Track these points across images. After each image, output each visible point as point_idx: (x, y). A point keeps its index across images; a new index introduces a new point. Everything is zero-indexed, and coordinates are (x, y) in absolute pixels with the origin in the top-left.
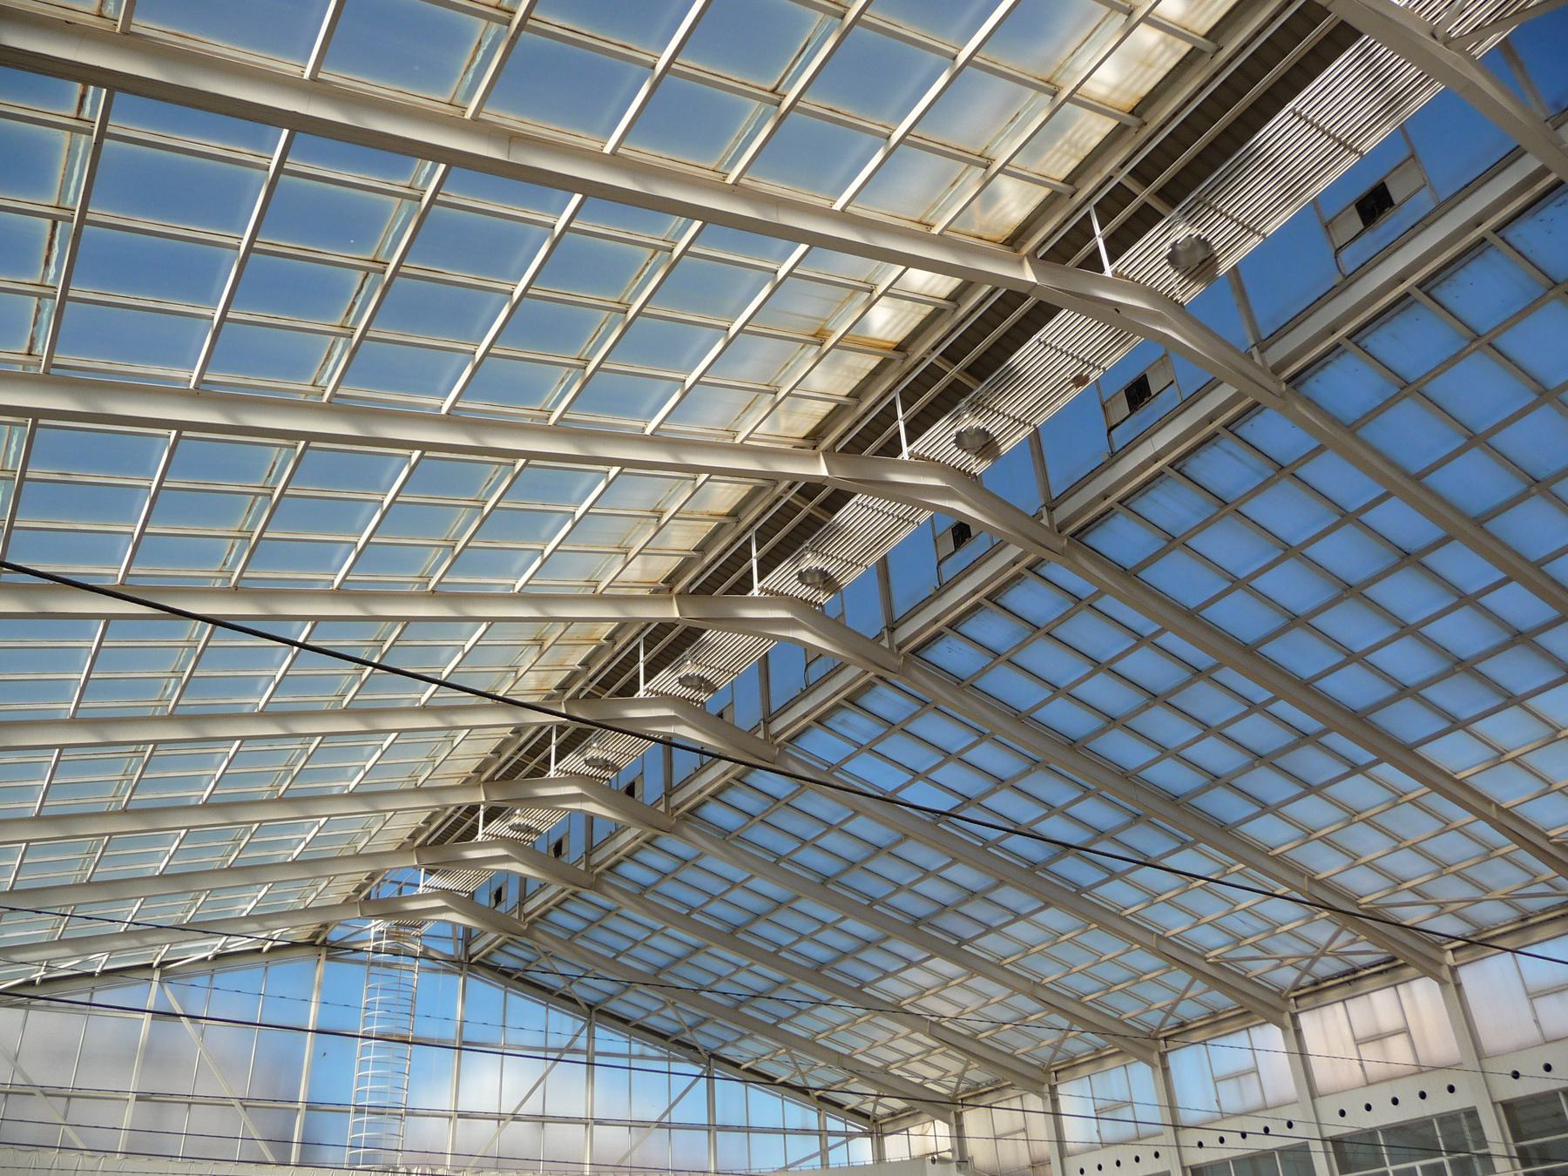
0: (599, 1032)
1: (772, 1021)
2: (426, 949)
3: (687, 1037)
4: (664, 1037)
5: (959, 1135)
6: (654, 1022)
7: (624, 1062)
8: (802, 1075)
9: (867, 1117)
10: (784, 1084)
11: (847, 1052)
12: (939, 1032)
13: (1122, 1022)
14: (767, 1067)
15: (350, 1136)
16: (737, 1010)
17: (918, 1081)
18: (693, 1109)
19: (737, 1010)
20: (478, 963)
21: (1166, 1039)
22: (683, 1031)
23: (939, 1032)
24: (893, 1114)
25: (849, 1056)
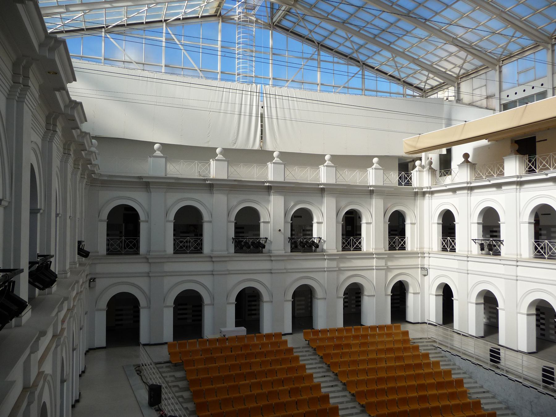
0: (322, 53)
1: (388, 44)
2: (257, 19)
3: (355, 55)
5: (458, 91)
6: (342, 49)
7: (332, 72)
9: (422, 90)
11: (416, 57)
13: (472, 47)
14: (384, 68)
15: (237, 72)
17: (444, 70)
20: (276, 25)
22: (353, 53)
24: (441, 84)
25: (417, 59)
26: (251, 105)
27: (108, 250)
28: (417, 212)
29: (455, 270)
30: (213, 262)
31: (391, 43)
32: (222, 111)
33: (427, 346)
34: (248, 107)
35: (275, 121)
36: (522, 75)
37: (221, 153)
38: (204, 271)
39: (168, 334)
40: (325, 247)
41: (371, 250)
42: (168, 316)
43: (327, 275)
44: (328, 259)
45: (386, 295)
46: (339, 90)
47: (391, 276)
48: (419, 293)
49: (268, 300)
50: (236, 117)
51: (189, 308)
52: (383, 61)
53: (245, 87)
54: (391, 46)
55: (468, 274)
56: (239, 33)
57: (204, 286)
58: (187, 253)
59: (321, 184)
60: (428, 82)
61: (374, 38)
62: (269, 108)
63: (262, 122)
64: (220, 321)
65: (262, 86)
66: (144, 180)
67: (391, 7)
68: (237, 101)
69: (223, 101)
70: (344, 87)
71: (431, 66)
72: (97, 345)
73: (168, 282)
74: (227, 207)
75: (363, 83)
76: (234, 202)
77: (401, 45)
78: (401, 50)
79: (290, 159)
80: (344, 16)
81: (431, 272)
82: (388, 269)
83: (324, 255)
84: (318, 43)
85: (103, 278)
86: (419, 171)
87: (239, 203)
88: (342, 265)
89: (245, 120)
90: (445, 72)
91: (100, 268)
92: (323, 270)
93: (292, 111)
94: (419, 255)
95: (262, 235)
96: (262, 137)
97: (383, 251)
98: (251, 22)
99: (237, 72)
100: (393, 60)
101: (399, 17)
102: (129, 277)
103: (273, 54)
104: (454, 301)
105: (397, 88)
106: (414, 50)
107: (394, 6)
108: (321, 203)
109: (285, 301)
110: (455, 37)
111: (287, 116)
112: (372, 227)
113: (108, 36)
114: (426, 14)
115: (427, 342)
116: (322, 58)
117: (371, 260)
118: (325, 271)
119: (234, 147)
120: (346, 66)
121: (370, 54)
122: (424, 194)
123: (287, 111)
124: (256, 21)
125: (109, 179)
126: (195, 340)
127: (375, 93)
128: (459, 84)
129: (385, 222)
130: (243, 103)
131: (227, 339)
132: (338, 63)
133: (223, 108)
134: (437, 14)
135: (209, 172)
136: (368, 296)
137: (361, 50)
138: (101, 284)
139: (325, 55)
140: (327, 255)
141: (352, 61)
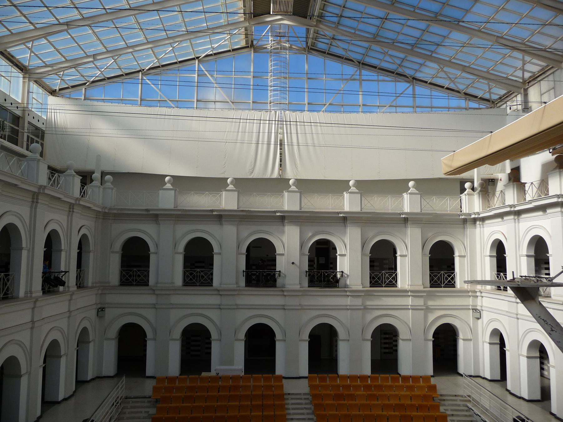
0: (364, 72)
2: (291, 45)
3: (400, 70)
4: (393, 73)
11: (467, 65)
13: (524, 44)
15: (269, 100)
16: (413, 48)
19: (413, 48)
24: (500, 98)
25: (469, 67)
26: (270, 133)
27: (184, 281)
28: (467, 243)
29: (505, 313)
30: (221, 295)
31: (432, 52)
33: (459, 405)
34: (266, 134)
35: (296, 147)
37: (354, 186)
38: (268, 305)
39: (304, 370)
40: (348, 283)
41: (407, 287)
42: (240, 350)
43: (352, 312)
44: (412, 296)
45: (364, 340)
46: (384, 109)
47: (432, 317)
48: (471, 340)
49: (281, 338)
50: (254, 146)
51: (196, 342)
52: (433, 73)
53: (257, 115)
54: (434, 55)
55: (518, 319)
56: (271, 61)
57: (212, 320)
58: (197, 286)
59: (403, 214)
60: (492, 91)
61: (412, 49)
62: (289, 134)
63: (281, 149)
64: (354, 358)
66: (151, 212)
67: (415, 12)
68: (255, 130)
69: (240, 131)
70: (390, 106)
71: (488, 72)
72: (104, 374)
73: (174, 315)
74: (237, 239)
75: (414, 101)
76: (245, 233)
77: (444, 53)
78: (447, 59)
79: (306, 186)
80: (373, 30)
81: (485, 315)
82: (428, 310)
83: (346, 291)
84: (359, 63)
85: (112, 307)
86: (468, 194)
87: (251, 234)
88: (368, 303)
89: (262, 149)
91: (111, 298)
92: (345, 307)
93: (314, 135)
94: (470, 294)
96: (281, 165)
97: (421, 288)
98: (285, 48)
99: (269, 100)
100: (442, 70)
101: (428, 23)
102: (139, 308)
103: (308, 78)
104: (507, 352)
105: (457, 102)
106: (460, 56)
107: (417, 11)
108: (345, 233)
109: (300, 340)
111: (310, 142)
112: (407, 260)
113: (145, 78)
114: (457, 14)
115: (461, 401)
116: (364, 78)
118: (409, 309)
119: (251, 177)
120: (394, 83)
121: (416, 67)
122: (475, 220)
123: (309, 136)
124: (290, 48)
125: (119, 212)
126: (378, 375)
127: (430, 109)
128: (526, 90)
129: (363, 254)
130: (261, 131)
131: (220, 378)
132: (384, 81)
133: (239, 138)
134: (467, 11)
135: (220, 203)
136: (403, 340)
137: (404, 64)
138: (110, 313)
139: (367, 73)
140: (350, 291)
141: (403, 77)
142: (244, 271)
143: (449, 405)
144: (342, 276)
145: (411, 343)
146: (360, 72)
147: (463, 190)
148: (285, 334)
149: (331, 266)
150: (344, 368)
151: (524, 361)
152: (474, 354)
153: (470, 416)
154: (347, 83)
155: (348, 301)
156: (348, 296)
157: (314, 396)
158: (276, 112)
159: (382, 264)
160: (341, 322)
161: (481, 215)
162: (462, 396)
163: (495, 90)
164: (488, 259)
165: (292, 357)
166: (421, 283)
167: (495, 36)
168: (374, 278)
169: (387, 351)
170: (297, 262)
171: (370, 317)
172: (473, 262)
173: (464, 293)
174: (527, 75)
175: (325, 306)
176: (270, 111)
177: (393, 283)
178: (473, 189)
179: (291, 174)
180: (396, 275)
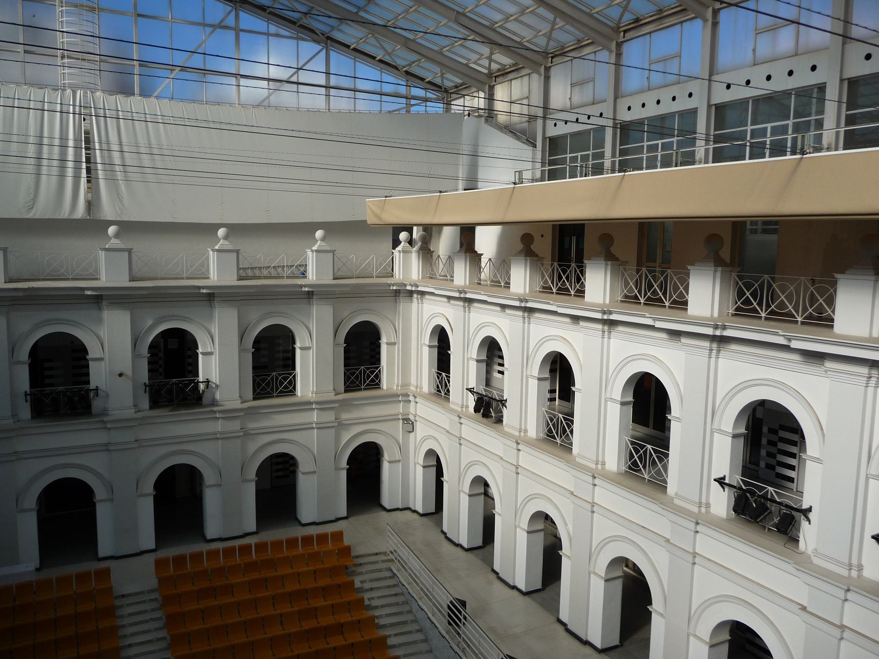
1: (355, 10)
3: (305, 21)
5: (491, 98)
8: (389, 54)
10: (381, 61)
12: (463, 20)
13: (494, 30)
18: (231, 21)
21: (625, 32)
23: (463, 20)
24: (456, 87)
31: (359, 8)
32: (15, 138)
36: (577, 89)
40: (218, 396)
43: (223, 444)
45: (245, 481)
47: (346, 437)
48: (399, 461)
58: (360, 390)
64: (229, 510)
65: (85, 96)
68: (32, 131)
71: (441, 53)
81: (419, 426)
82: (341, 426)
83: (215, 412)
86: (404, 252)
87: (35, 328)
89: (50, 171)
90: (467, 65)
95: (92, 386)
97: (331, 396)
108: (211, 317)
110: (461, 10)
117: (308, 413)
122: (411, 293)
128: (492, 88)
129: (336, 345)
132: (277, 35)
136: (303, 474)
142: (26, 394)
143: (368, 572)
144: (207, 386)
145: (315, 476)
146: (237, 17)
147: (396, 243)
148: (111, 488)
149: (190, 368)
150: (213, 527)
151: (465, 500)
152: (403, 482)
153: (394, 586)
154: (212, 32)
155: (219, 426)
156: (218, 418)
157: (167, 600)
158: (74, 93)
159: (271, 362)
160: (206, 457)
161: (420, 289)
162: (385, 553)
163: (448, 76)
164: (426, 350)
165: (126, 522)
166: (331, 387)
167: (454, 10)
168: (259, 385)
169: (281, 473)
170: (128, 371)
171: (253, 446)
172: (405, 360)
173: (393, 398)
174: (494, 66)
175: (183, 437)
176: (64, 90)
177: (290, 389)
178: (411, 242)
179: (108, 210)
180: (294, 377)
